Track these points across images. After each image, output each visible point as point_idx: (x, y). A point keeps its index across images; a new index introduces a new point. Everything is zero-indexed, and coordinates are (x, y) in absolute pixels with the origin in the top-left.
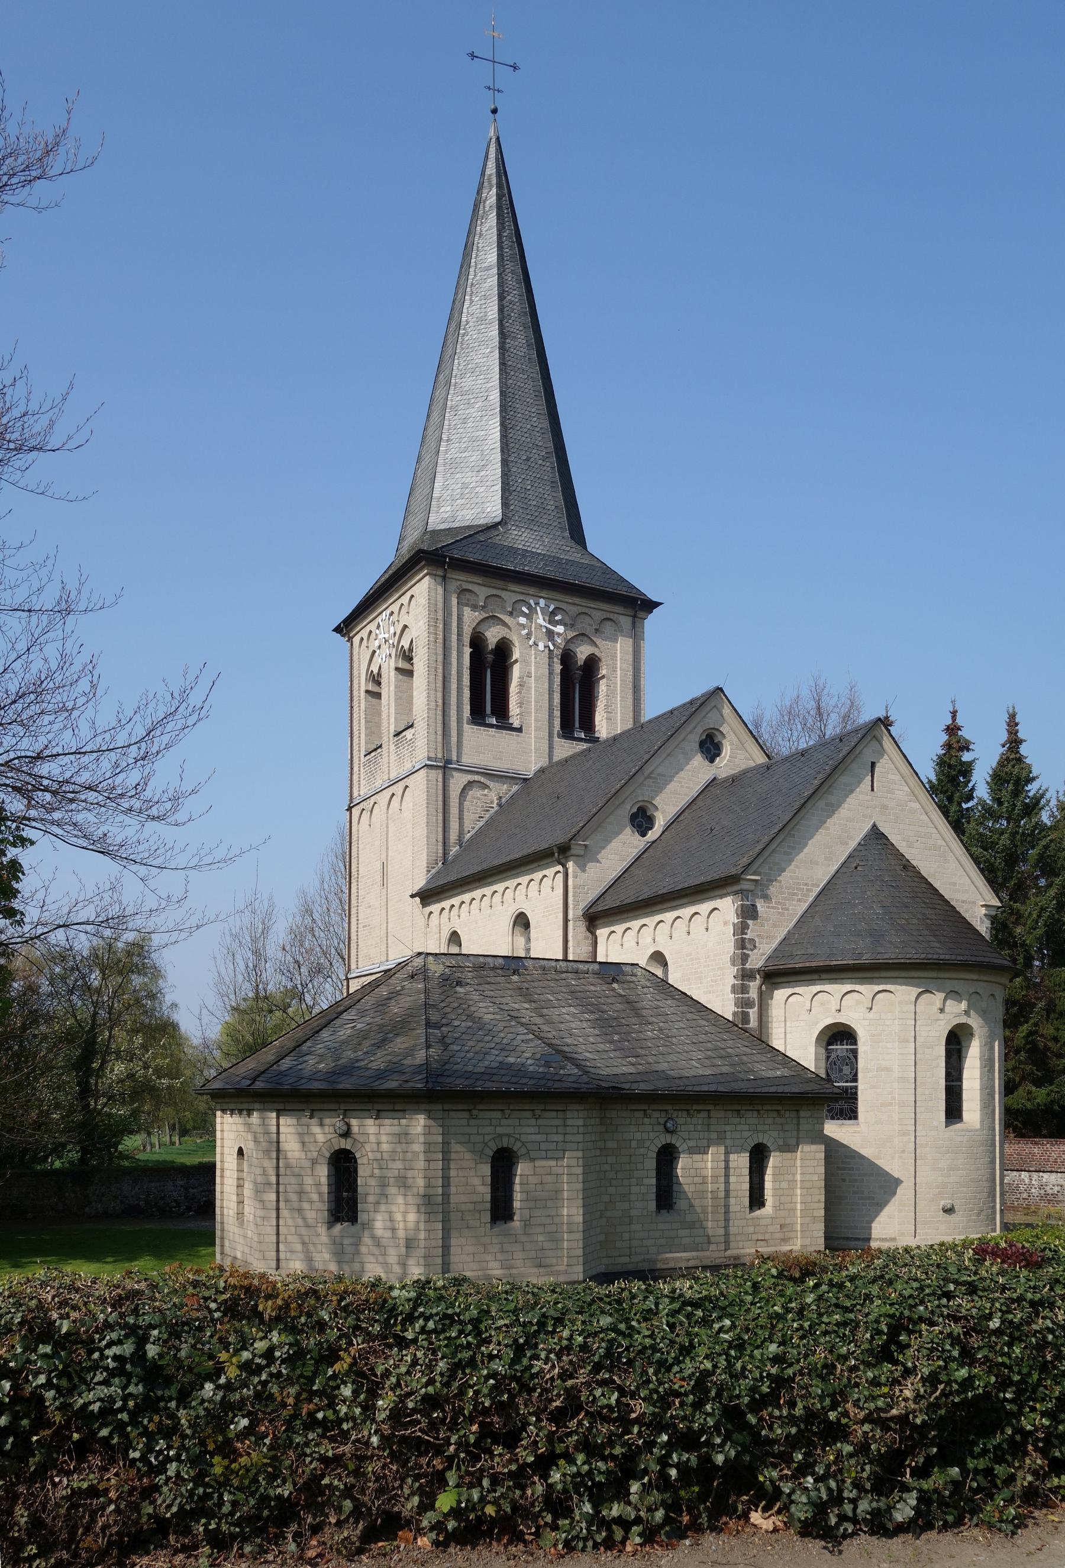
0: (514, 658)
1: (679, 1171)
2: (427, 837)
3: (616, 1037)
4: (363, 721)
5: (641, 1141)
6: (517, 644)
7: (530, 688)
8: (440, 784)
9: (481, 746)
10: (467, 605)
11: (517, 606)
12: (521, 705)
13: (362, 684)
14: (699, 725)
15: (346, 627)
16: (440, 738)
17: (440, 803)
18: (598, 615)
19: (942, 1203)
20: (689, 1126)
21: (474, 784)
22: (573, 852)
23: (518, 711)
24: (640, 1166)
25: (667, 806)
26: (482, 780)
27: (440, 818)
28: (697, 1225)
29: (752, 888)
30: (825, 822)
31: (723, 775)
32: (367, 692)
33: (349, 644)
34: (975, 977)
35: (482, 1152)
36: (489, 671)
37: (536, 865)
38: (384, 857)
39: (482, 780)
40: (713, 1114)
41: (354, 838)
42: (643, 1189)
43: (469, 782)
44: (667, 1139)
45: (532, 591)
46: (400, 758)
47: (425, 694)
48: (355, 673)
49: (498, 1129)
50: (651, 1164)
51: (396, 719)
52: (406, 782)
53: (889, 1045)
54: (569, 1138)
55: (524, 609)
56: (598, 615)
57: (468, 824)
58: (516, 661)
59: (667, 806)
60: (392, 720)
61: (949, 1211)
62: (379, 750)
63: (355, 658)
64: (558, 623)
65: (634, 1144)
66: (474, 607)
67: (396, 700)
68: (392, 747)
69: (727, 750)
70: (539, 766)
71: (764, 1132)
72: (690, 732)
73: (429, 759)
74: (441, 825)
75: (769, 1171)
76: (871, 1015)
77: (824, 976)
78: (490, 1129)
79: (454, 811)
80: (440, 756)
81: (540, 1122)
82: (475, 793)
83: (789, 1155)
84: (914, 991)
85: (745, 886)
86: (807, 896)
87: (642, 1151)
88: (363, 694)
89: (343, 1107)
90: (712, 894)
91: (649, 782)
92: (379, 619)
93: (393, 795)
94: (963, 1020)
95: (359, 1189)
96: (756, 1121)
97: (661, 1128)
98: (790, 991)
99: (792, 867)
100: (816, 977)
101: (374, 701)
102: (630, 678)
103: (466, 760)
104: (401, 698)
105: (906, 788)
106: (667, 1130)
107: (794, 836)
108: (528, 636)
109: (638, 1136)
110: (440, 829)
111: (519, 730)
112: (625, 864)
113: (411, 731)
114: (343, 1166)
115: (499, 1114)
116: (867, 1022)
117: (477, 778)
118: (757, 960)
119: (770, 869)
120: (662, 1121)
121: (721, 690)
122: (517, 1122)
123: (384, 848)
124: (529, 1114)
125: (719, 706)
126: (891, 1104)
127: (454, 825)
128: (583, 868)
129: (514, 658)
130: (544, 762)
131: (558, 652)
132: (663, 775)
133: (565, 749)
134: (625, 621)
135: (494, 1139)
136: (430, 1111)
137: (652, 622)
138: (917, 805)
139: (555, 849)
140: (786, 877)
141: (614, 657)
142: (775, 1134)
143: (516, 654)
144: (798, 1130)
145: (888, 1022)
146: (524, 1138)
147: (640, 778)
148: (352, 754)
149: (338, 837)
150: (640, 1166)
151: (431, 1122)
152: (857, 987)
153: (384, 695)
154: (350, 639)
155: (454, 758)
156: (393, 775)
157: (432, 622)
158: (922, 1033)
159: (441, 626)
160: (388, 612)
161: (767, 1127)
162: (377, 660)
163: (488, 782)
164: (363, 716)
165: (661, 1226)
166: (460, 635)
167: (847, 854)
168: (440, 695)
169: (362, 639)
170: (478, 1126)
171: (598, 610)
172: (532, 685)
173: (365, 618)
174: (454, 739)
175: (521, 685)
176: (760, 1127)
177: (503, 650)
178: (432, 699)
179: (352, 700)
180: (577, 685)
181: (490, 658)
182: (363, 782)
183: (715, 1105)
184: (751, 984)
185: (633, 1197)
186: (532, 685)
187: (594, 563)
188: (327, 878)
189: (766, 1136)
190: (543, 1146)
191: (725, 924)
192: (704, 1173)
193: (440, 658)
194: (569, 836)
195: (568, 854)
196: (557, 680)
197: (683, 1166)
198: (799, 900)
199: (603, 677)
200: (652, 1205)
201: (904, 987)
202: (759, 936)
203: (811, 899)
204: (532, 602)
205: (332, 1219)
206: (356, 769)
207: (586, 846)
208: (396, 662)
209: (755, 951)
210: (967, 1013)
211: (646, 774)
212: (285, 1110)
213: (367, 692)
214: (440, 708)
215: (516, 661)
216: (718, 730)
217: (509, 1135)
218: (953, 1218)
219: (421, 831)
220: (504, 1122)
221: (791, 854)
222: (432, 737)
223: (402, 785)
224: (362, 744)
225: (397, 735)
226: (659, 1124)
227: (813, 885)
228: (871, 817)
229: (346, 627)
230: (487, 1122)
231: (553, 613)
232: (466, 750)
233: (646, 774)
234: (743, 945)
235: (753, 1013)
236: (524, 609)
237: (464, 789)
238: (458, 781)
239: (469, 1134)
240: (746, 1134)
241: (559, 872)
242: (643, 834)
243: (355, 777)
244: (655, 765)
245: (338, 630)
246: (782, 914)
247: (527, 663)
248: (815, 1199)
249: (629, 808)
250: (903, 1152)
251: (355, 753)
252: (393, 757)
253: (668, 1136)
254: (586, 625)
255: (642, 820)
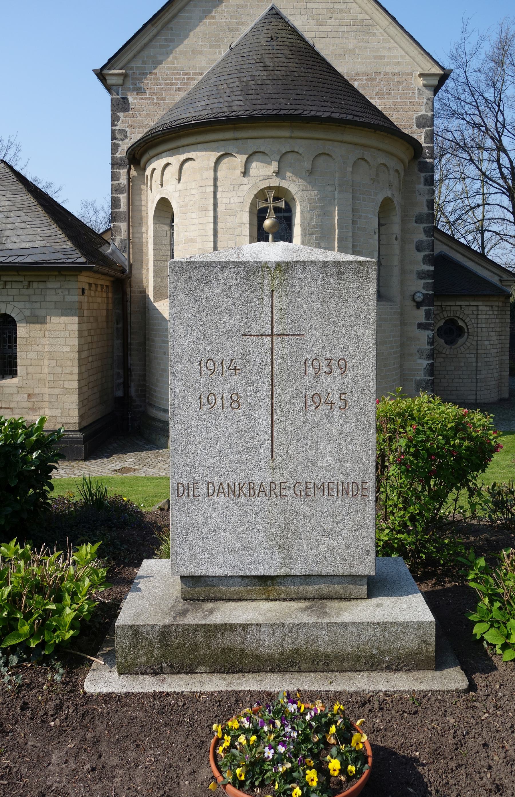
30: (211, 12)
34: (286, 133)
71: (7, 303)
83: (38, 326)
84: (213, 156)
94: (275, 182)
99: (170, 59)
107: (172, 29)
119: (144, 63)
140: (163, 70)
142: (21, 305)
158: (223, 198)
198: (179, 89)
201: (204, 153)
202: (130, 126)
209: (126, 141)
210: (278, 173)
221: (169, 46)
227: (196, 74)
235: (123, 198)
246: (158, 104)
248: (67, 370)
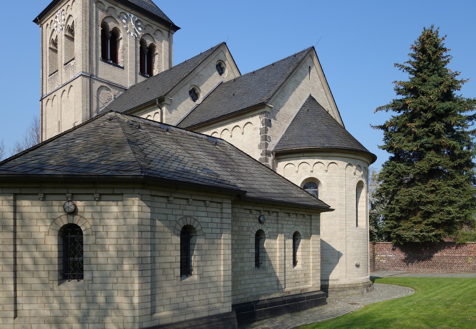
0: (120, 37)
1: (265, 245)
2: (82, 107)
3: (229, 170)
4: (48, 61)
5: (248, 227)
6: (121, 31)
7: (127, 51)
8: (88, 84)
9: (106, 71)
10: (100, 8)
11: (122, 15)
12: (123, 57)
13: (47, 44)
14: (216, 57)
15: (40, 19)
16: (88, 64)
17: (88, 93)
18: (155, 28)
19: (356, 262)
20: (270, 219)
21: (103, 88)
22: (166, 102)
23: (122, 60)
24: (248, 242)
25: (205, 90)
26: (107, 86)
27: (88, 100)
28: (273, 275)
29: (270, 111)
31: (225, 80)
32: (50, 48)
33: (41, 28)
35: (175, 227)
36: (109, 41)
37: (144, 110)
38: (59, 119)
39: (107, 86)
40: (280, 214)
41: (44, 112)
42: (250, 255)
43: (101, 86)
44: (259, 227)
45: (128, 9)
46: (67, 74)
47: (81, 43)
48: (44, 40)
49: (184, 211)
50: (253, 241)
51: (65, 57)
52: (71, 84)
53: (335, 188)
54: (224, 221)
55: (125, 16)
56: (155, 28)
57: (101, 105)
58: (121, 38)
59: (205, 90)
60: (63, 58)
61: (358, 266)
62: (56, 73)
63: (44, 34)
64: (139, 26)
65: (245, 229)
66: (103, 10)
67: (65, 49)
68: (63, 70)
69: (227, 71)
70: (131, 85)
71: (298, 225)
72: (213, 60)
73: (83, 72)
74: (88, 102)
75: (300, 246)
76: (327, 174)
77: (305, 155)
78: (179, 212)
79: (95, 99)
80: (88, 72)
81: (208, 209)
82: (104, 92)
84: (346, 164)
85: (267, 109)
86: (288, 120)
87: (249, 233)
88: (48, 49)
89: (71, 191)
90: (247, 115)
91: (197, 77)
92: (56, 14)
93: (64, 90)
95: (85, 254)
96: (294, 219)
97: (257, 221)
98: (287, 162)
100: (301, 155)
101: (54, 53)
102: (167, 56)
103: (100, 76)
104: (67, 49)
105: (320, 82)
106: (260, 222)
108: (127, 29)
109: (247, 224)
110: (88, 105)
111: (123, 68)
112: (187, 112)
113: (74, 61)
114: (71, 239)
115: (185, 202)
116: (325, 177)
117: (105, 85)
118: (271, 148)
120: (258, 216)
121: (225, 43)
122: (195, 208)
123: (59, 115)
124: (202, 203)
125: (224, 51)
126: (335, 216)
127: (95, 104)
128: (170, 111)
129: (120, 37)
130: (133, 83)
131: (139, 39)
132: (203, 76)
133: (141, 79)
134: (166, 33)
135: (182, 218)
136: (142, 195)
137: (176, 35)
138: (323, 90)
139: (157, 100)
141: (161, 47)
142: (302, 227)
143: (121, 35)
144: (311, 226)
145: (334, 178)
146: (199, 219)
147: (193, 74)
148: (42, 76)
149: (34, 122)
150: (248, 242)
151: (143, 204)
152: (321, 161)
153: (59, 50)
154: (42, 26)
155: (95, 74)
156: (64, 82)
157: (84, 12)
159: (88, 14)
160: (61, 10)
161: (299, 223)
162: (55, 34)
163: (110, 88)
164: (48, 59)
165: (258, 276)
166: (97, 20)
167: (301, 105)
168: (88, 45)
169: (48, 25)
170: (172, 209)
171: (156, 26)
172: (127, 49)
173: (49, 14)
174: (94, 66)
175: (124, 49)
176: (297, 223)
177: (115, 33)
178: (84, 45)
179: (42, 52)
180: (146, 55)
181: (110, 35)
182: (48, 88)
183: (281, 209)
184: (269, 158)
185: (245, 260)
186: (127, 49)
187: (154, 5)
188: (29, 139)
189: (299, 228)
190: (210, 225)
191: (255, 129)
192: (275, 246)
193: (88, 28)
194: (165, 92)
195: (163, 103)
196: (139, 50)
197: (267, 243)
198: (286, 122)
199: (157, 54)
200: (178, 271)
203: (290, 122)
204: (128, 14)
205: (61, 277)
206: (44, 82)
207: (171, 100)
208: (65, 32)
209: (271, 142)
211: (196, 73)
212: (21, 194)
213: (50, 48)
214: (88, 50)
215: (121, 38)
216: (223, 61)
217: (190, 217)
218: (360, 269)
219: (79, 105)
220: (188, 208)
222: (85, 63)
223: (68, 86)
224: (47, 71)
225: (66, 64)
226: (256, 218)
227: (291, 116)
228: (309, 91)
229: (40, 19)
230: (178, 207)
231: (137, 22)
232: (100, 72)
233: (196, 73)
234: (265, 138)
236: (125, 16)
237: (99, 89)
238: (97, 85)
239: (167, 214)
240: (292, 226)
241: (157, 113)
242: (194, 100)
243: (44, 86)
244: (200, 70)
245: (36, 21)
247: (126, 40)
249: (188, 88)
250: (341, 238)
251: (44, 75)
252: (63, 75)
253: (260, 225)
254: (149, 30)
255: (194, 95)
